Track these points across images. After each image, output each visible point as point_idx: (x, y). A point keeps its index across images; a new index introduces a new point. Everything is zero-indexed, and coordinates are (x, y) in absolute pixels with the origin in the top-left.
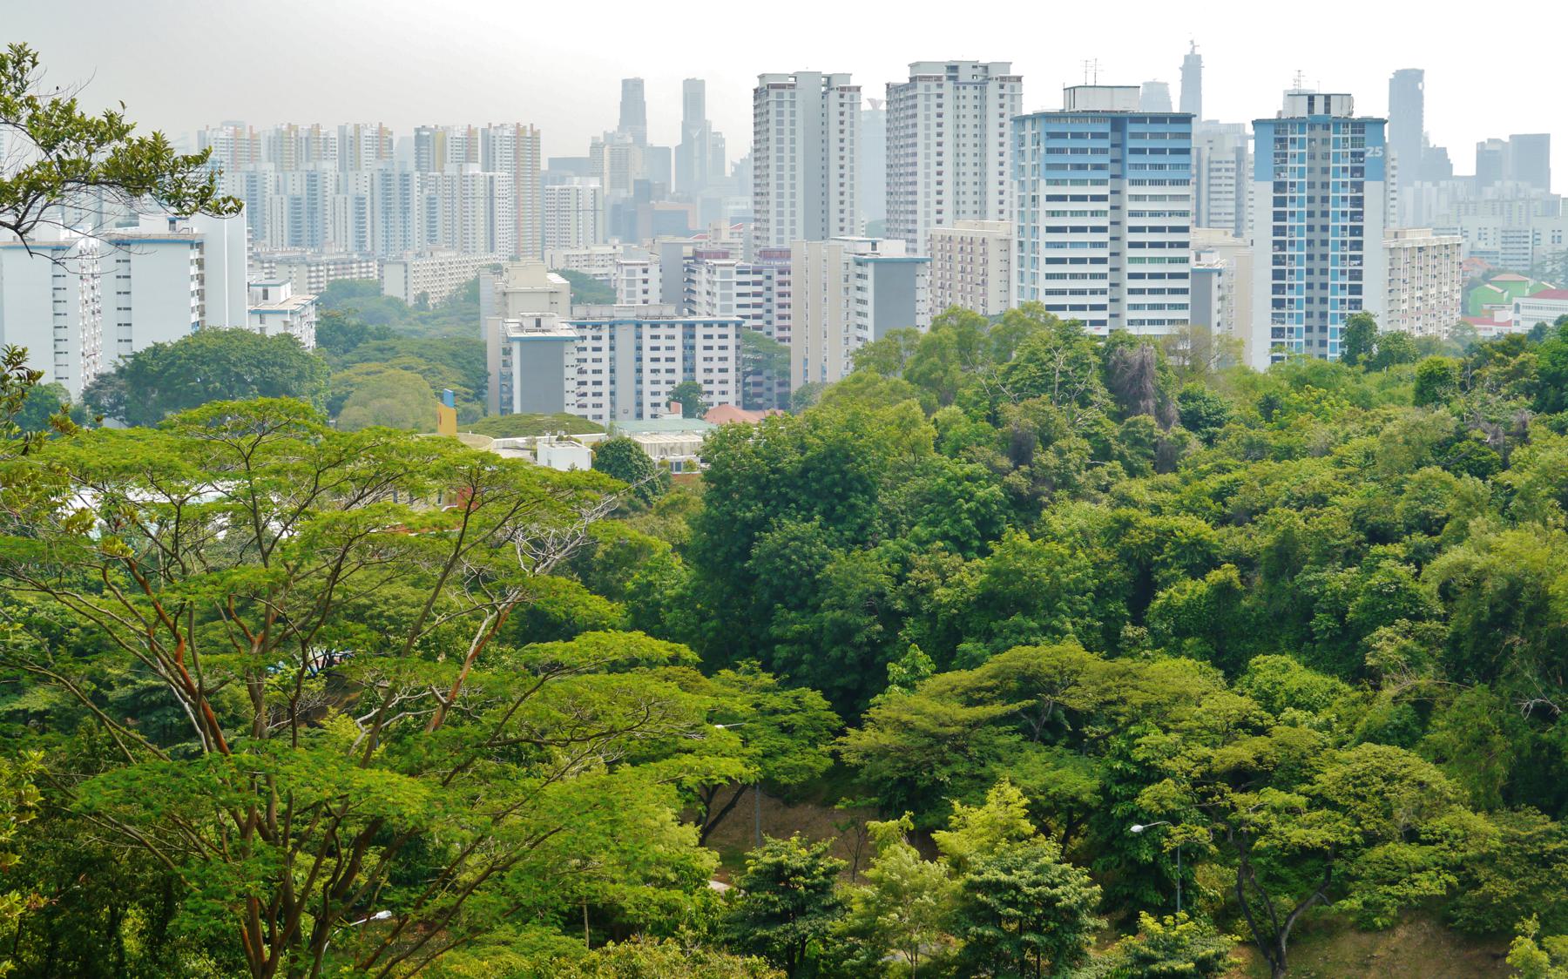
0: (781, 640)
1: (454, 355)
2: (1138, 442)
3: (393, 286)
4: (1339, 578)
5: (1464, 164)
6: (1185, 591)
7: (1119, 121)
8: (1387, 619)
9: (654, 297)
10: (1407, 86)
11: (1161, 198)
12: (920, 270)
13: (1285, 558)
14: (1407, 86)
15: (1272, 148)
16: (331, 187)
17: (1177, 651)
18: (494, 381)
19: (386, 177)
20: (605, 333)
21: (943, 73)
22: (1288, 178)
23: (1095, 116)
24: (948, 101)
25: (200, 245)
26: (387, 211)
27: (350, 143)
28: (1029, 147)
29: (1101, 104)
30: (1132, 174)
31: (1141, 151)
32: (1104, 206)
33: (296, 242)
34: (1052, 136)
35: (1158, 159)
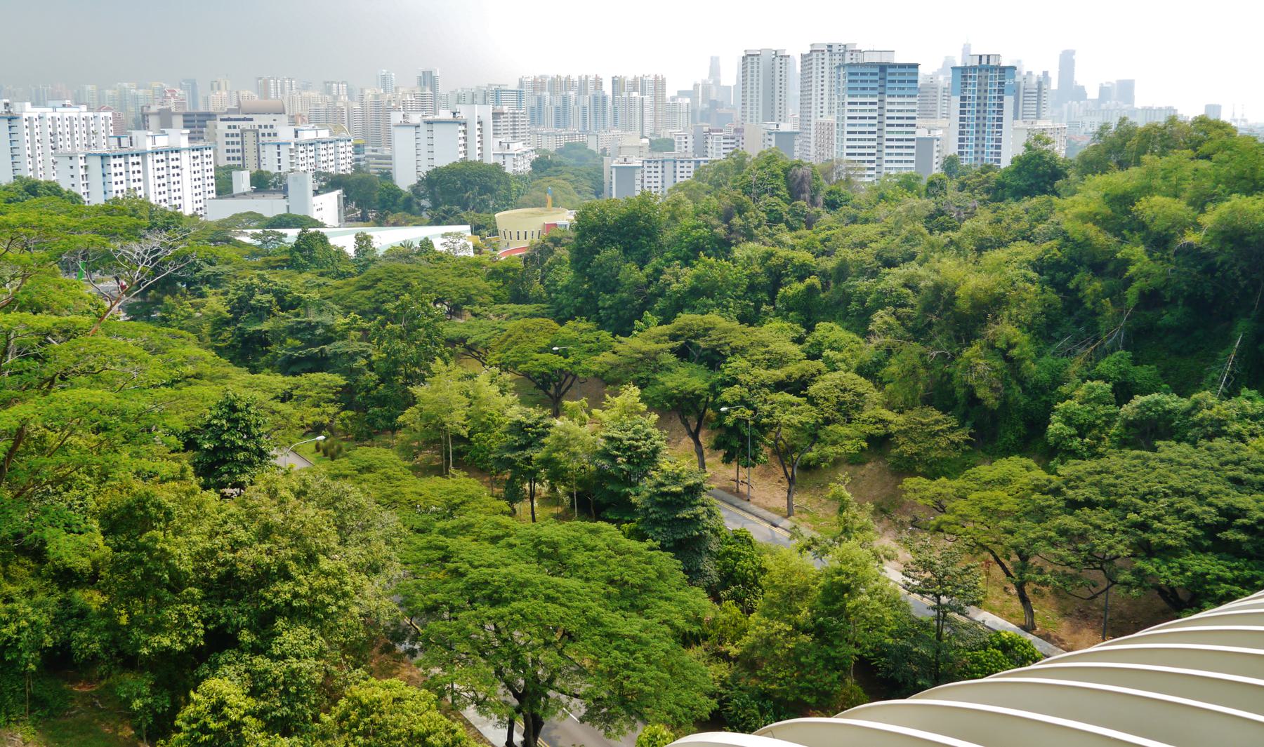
0: (604, 308)
1: (589, 174)
2: (797, 214)
3: (592, 146)
4: (863, 284)
5: (1093, 94)
6: (795, 288)
7: (883, 67)
8: (882, 306)
9: (690, 149)
10: (1067, 61)
11: (903, 103)
12: (797, 137)
13: (842, 272)
14: (1067, 61)
15: (960, 80)
16: (547, 103)
17: (786, 318)
18: (606, 186)
19: (596, 98)
20: (660, 165)
21: (825, 48)
22: (967, 94)
23: (872, 65)
24: (827, 61)
25: (465, 124)
26: (596, 112)
27: (583, 83)
28: (842, 79)
29: (876, 59)
30: (889, 92)
31: (893, 81)
32: (876, 107)
33: (558, 126)
34: (851, 74)
35: (902, 85)
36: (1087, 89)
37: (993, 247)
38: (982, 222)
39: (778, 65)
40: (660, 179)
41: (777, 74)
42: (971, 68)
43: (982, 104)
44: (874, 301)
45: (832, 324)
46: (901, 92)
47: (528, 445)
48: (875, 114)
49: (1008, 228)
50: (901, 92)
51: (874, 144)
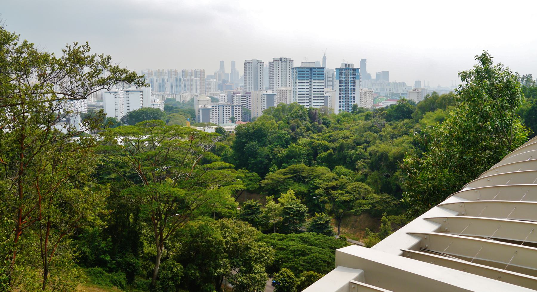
3: (178, 99)
4: (351, 152)
5: (374, 77)
6: (323, 154)
7: (311, 69)
9: (226, 101)
13: (341, 148)
14: (324, 59)
15: (339, 73)
16: (166, 81)
18: (197, 116)
19: (177, 79)
20: (217, 108)
24: (280, 65)
26: (177, 85)
28: (295, 73)
29: (308, 65)
30: (313, 78)
32: (308, 84)
33: (160, 91)
34: (299, 71)
35: (318, 76)
36: (371, 75)
37: (396, 138)
38: (389, 129)
39: (259, 66)
40: (217, 114)
41: (259, 70)
42: (343, 69)
43: (347, 83)
44: (355, 157)
45: (341, 167)
46: (318, 78)
47: (254, 213)
48: (308, 87)
49: (399, 130)
50: (318, 78)
51: (308, 98)
